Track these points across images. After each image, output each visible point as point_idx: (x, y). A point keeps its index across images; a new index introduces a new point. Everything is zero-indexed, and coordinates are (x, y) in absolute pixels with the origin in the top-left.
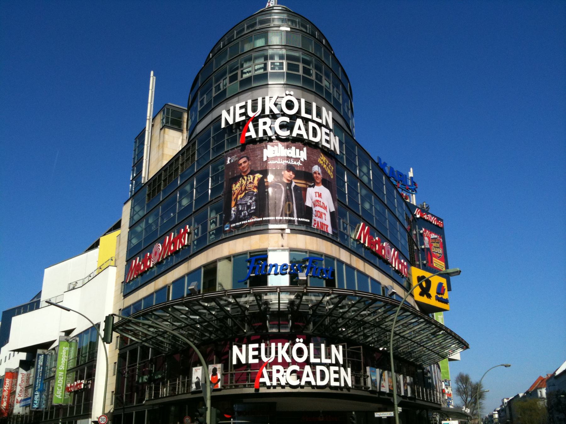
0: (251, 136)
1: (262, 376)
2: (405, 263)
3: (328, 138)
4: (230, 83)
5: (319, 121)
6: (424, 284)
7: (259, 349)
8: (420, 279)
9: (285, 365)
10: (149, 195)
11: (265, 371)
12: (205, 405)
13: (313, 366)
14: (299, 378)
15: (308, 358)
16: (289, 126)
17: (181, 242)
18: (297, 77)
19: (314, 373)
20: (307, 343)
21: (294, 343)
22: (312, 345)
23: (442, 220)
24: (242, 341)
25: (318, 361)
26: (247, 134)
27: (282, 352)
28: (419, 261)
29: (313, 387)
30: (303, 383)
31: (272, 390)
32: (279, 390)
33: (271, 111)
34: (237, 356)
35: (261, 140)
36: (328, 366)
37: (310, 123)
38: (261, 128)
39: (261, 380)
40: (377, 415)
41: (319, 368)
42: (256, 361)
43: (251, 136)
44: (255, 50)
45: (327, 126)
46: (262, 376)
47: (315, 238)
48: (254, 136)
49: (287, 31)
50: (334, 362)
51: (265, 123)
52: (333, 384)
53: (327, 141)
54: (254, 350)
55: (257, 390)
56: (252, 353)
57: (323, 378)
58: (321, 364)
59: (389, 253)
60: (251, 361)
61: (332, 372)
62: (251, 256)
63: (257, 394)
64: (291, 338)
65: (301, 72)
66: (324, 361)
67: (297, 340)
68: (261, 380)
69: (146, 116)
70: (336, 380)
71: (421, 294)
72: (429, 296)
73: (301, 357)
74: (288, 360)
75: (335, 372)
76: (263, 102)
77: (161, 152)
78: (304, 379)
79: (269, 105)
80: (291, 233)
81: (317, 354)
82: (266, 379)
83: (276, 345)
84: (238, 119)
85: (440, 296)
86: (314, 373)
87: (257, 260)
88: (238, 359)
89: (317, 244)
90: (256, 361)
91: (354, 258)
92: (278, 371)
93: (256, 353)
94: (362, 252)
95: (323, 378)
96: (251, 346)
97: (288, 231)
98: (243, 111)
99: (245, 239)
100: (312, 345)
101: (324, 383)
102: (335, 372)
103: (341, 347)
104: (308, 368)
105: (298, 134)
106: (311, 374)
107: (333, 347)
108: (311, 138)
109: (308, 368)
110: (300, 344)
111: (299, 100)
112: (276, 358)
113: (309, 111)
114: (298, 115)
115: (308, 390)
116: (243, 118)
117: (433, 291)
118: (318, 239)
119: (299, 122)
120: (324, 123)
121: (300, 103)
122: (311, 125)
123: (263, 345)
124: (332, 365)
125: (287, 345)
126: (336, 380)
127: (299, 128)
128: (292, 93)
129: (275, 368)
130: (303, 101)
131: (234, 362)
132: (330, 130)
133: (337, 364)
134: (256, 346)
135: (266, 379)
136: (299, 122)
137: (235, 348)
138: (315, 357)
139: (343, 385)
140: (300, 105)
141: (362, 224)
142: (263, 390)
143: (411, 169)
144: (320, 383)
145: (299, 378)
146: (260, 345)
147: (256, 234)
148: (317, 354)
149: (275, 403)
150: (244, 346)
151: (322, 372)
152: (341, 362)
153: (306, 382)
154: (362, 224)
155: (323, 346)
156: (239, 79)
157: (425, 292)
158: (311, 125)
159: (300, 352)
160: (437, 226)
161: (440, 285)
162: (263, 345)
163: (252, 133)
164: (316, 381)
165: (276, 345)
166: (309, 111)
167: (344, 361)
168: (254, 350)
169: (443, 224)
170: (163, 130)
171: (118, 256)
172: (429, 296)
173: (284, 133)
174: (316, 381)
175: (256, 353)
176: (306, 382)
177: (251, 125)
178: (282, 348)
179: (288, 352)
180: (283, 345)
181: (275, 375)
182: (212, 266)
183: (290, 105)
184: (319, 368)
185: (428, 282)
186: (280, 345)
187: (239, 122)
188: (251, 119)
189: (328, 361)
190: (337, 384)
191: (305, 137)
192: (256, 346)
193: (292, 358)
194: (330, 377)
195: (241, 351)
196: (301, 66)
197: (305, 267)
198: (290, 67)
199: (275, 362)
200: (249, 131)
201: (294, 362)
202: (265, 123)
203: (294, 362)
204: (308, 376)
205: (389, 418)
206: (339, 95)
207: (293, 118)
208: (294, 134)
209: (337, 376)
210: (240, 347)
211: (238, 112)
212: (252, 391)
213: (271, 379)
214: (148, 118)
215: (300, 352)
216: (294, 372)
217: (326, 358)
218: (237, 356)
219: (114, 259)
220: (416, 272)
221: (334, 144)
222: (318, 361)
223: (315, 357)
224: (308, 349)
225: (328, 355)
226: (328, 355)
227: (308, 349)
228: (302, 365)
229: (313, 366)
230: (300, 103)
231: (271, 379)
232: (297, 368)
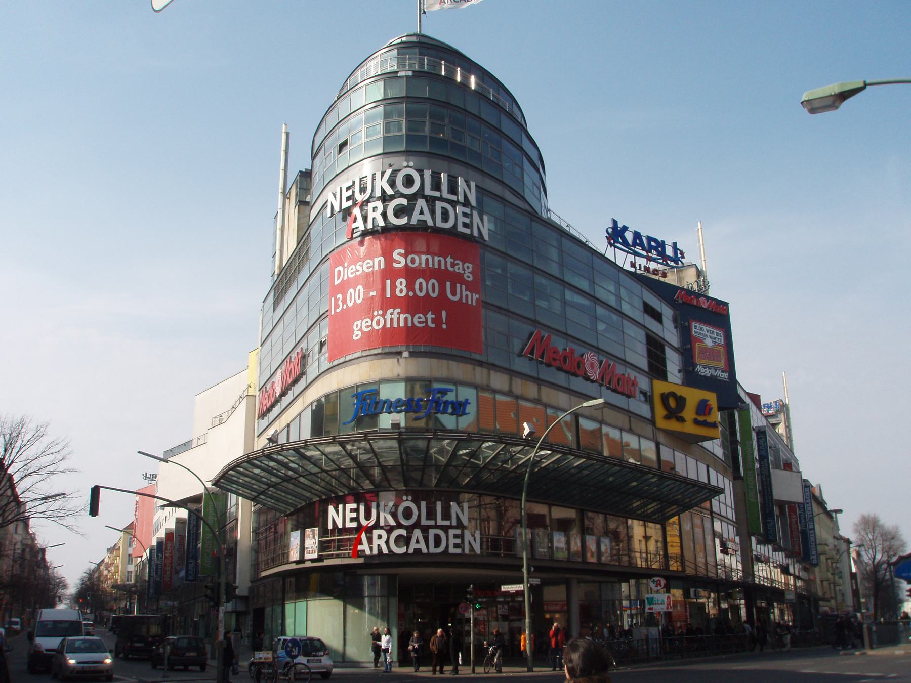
5: (453, 198)
6: (672, 403)
7: (357, 510)
14: (408, 545)
19: (433, 212)
20: (416, 501)
22: (423, 504)
24: (340, 500)
25: (437, 194)
30: (411, 551)
33: (383, 191)
36: (445, 529)
37: (437, 202)
38: (376, 542)
40: (504, 588)
41: (432, 532)
45: (466, 203)
49: (407, 77)
50: (454, 523)
52: (452, 550)
56: (349, 515)
58: (436, 527)
60: (349, 525)
66: (440, 522)
72: (682, 420)
74: (389, 191)
78: (413, 546)
81: (431, 515)
85: (701, 418)
90: (354, 525)
92: (380, 537)
96: (350, 506)
97: (406, 354)
98: (354, 515)
100: (423, 504)
106: (426, 210)
108: (440, 224)
109: (417, 533)
111: (421, 172)
113: (436, 186)
117: (689, 413)
119: (421, 203)
121: (422, 176)
124: (451, 527)
128: (411, 164)
129: (376, 533)
130: (427, 174)
131: (330, 527)
134: (354, 506)
138: (443, 519)
139: (467, 551)
148: (431, 515)
150: (341, 506)
158: (439, 205)
166: (436, 186)
172: (682, 420)
182: (373, 387)
189: (447, 523)
191: (430, 223)
192: (354, 506)
194: (450, 543)
195: (337, 512)
199: (377, 526)
202: (380, 537)
203: (399, 526)
204: (417, 542)
207: (412, 198)
208: (414, 222)
211: (349, 515)
222: (432, 523)
223: (443, 519)
224: (419, 510)
226: (447, 515)
227: (419, 510)
229: (425, 530)
230: (422, 176)
232: (403, 532)
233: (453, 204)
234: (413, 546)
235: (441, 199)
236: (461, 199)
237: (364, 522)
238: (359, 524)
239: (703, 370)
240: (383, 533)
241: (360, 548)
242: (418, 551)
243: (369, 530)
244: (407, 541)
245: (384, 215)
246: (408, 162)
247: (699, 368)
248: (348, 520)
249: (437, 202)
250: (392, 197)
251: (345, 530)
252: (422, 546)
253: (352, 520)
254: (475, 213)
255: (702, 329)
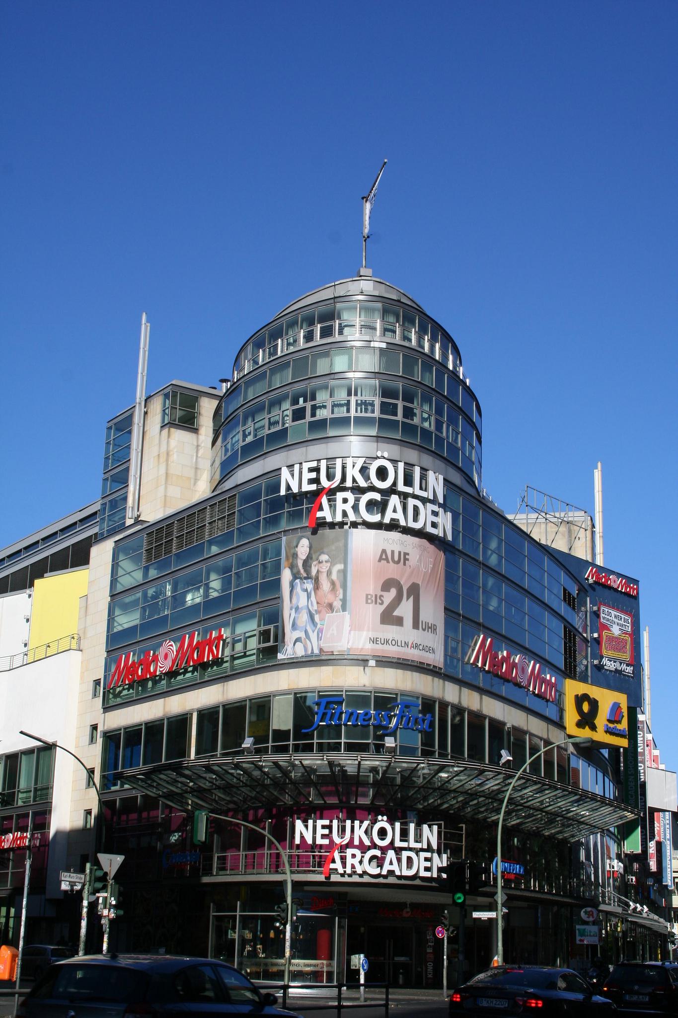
0: (324, 518)
1: (333, 861)
2: (553, 680)
3: (435, 519)
4: (293, 421)
5: (423, 494)
6: (586, 707)
7: (330, 827)
8: (580, 700)
9: (364, 849)
10: (149, 551)
11: (337, 855)
12: (286, 901)
13: (398, 851)
14: (380, 865)
15: (395, 484)
16: (381, 506)
17: (211, 650)
18: (393, 425)
19: (399, 860)
20: (391, 821)
21: (374, 822)
22: (398, 825)
23: (636, 582)
24: (308, 812)
25: (405, 845)
26: (319, 514)
27: (359, 832)
28: (586, 658)
29: (400, 877)
30: (384, 872)
31: (346, 879)
32: (355, 879)
34: (301, 833)
35: (342, 524)
36: (417, 851)
37: (410, 499)
38: (340, 506)
39: (332, 866)
40: (476, 915)
42: (326, 842)
43: (324, 518)
44: (332, 376)
46: (333, 861)
47: (409, 673)
48: (329, 519)
49: (381, 349)
50: (425, 847)
51: (345, 501)
52: (423, 874)
53: (434, 525)
54: (323, 827)
55: (328, 878)
56: (320, 831)
57: (415, 519)
59: (523, 670)
61: (422, 859)
62: (320, 697)
63: (328, 883)
64: (373, 811)
65: (400, 417)
66: (413, 844)
67: (380, 818)
68: (332, 866)
69: (135, 398)
70: (427, 869)
71: (580, 725)
72: (593, 728)
73: (383, 839)
74: (367, 842)
75: (426, 859)
76: (344, 468)
77: (162, 471)
78: (387, 867)
79: (353, 472)
80: (377, 666)
81: (404, 835)
82: (338, 865)
83: (353, 822)
84: (306, 487)
86: (399, 860)
87: (328, 703)
88: (302, 837)
89: (412, 681)
90: (326, 842)
91: (466, 691)
92: (354, 856)
93: (326, 832)
94: (481, 681)
95: (415, 519)
96: (320, 823)
98: (313, 475)
99: (312, 669)
101: (411, 873)
102: (426, 859)
103: (435, 828)
104: (391, 854)
105: (392, 520)
106: (400, 509)
107: (425, 827)
109: (391, 854)
110: (382, 822)
111: (394, 462)
112: (352, 839)
113: (408, 482)
114: (392, 490)
115: (391, 880)
116: (313, 487)
117: (601, 720)
118: (414, 673)
119: (394, 500)
120: (431, 497)
122: (411, 502)
123: (335, 822)
124: (422, 850)
125: (366, 823)
126: (427, 869)
127: (394, 510)
128: (386, 455)
129: (340, 496)
132: (440, 505)
133: (429, 849)
134: (327, 822)
135: (338, 865)
136: (394, 500)
137: (299, 824)
138: (401, 841)
140: (396, 474)
141: (482, 636)
142: (334, 878)
143: (599, 464)
144: (406, 872)
145: (380, 865)
146: (331, 822)
147: (327, 665)
148: (404, 835)
149: (346, 893)
150: (310, 822)
151: (409, 859)
152: (435, 846)
153: (389, 871)
154: (482, 636)
155: (412, 826)
156: (308, 418)
157: (587, 720)
158: (411, 502)
159: (382, 833)
160: (627, 594)
161: (616, 707)
162: (335, 822)
163: (326, 514)
164: (401, 870)
165: (353, 822)
166: (408, 482)
167: (439, 844)
168: (323, 827)
169: (637, 589)
170: (165, 431)
171: (84, 633)
172: (593, 728)
173: (375, 518)
174: (401, 870)
175: (326, 832)
176: (389, 871)
177: (324, 500)
178: (360, 826)
179: (366, 832)
180: (361, 822)
181: (349, 860)
183: (382, 473)
184: (405, 854)
185: (594, 704)
186: (357, 823)
187: (307, 493)
188: (325, 492)
189: (418, 845)
190: (428, 874)
191: (403, 523)
192: (327, 822)
193: (372, 841)
195: (306, 827)
196: (400, 404)
197: (395, 715)
198: (384, 408)
199: (350, 845)
200: (321, 509)
201: (374, 846)
202: (345, 501)
203: (374, 846)
204: (391, 863)
205: (490, 919)
206: (457, 433)
208: (387, 520)
209: (428, 864)
210: (305, 822)
211: (307, 476)
212: (321, 878)
213: (344, 865)
214: (138, 400)
215: (382, 833)
216: (373, 857)
217: (416, 841)
218: (301, 833)
219: (76, 636)
220: (573, 688)
221: (445, 525)
222: (405, 845)
223: (401, 841)
224: (393, 829)
225: (418, 839)
226: (418, 839)
227: (393, 829)
228: (384, 850)
229: (398, 851)
231: (344, 865)
232: (378, 853)
233: (424, 501)
234: (387, 867)
235: (415, 497)
236: (431, 497)
237: (337, 840)
238: (332, 841)
239: (608, 663)
240: (358, 852)
241: (319, 514)
242: (391, 873)
243: (332, 492)
244: (380, 862)
245: (355, 508)
246: (382, 452)
247: (605, 661)
248: (318, 836)
249: (410, 499)
250: (369, 848)
251: (314, 846)
252: (395, 867)
253: (311, 481)
254: (435, 855)
255: (609, 614)
